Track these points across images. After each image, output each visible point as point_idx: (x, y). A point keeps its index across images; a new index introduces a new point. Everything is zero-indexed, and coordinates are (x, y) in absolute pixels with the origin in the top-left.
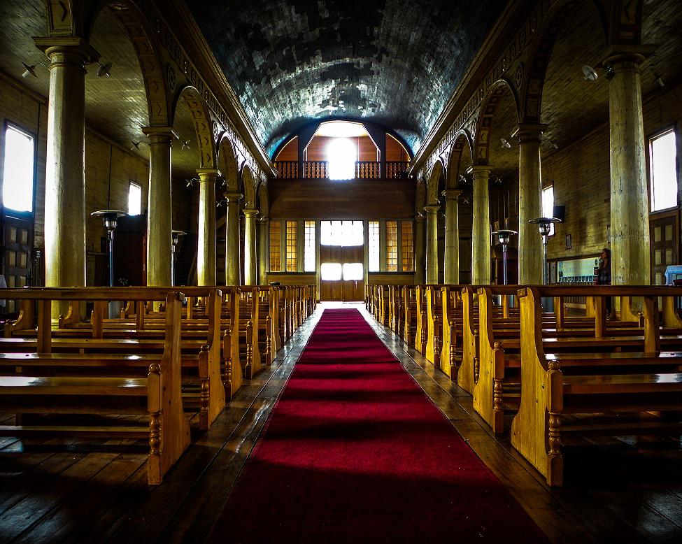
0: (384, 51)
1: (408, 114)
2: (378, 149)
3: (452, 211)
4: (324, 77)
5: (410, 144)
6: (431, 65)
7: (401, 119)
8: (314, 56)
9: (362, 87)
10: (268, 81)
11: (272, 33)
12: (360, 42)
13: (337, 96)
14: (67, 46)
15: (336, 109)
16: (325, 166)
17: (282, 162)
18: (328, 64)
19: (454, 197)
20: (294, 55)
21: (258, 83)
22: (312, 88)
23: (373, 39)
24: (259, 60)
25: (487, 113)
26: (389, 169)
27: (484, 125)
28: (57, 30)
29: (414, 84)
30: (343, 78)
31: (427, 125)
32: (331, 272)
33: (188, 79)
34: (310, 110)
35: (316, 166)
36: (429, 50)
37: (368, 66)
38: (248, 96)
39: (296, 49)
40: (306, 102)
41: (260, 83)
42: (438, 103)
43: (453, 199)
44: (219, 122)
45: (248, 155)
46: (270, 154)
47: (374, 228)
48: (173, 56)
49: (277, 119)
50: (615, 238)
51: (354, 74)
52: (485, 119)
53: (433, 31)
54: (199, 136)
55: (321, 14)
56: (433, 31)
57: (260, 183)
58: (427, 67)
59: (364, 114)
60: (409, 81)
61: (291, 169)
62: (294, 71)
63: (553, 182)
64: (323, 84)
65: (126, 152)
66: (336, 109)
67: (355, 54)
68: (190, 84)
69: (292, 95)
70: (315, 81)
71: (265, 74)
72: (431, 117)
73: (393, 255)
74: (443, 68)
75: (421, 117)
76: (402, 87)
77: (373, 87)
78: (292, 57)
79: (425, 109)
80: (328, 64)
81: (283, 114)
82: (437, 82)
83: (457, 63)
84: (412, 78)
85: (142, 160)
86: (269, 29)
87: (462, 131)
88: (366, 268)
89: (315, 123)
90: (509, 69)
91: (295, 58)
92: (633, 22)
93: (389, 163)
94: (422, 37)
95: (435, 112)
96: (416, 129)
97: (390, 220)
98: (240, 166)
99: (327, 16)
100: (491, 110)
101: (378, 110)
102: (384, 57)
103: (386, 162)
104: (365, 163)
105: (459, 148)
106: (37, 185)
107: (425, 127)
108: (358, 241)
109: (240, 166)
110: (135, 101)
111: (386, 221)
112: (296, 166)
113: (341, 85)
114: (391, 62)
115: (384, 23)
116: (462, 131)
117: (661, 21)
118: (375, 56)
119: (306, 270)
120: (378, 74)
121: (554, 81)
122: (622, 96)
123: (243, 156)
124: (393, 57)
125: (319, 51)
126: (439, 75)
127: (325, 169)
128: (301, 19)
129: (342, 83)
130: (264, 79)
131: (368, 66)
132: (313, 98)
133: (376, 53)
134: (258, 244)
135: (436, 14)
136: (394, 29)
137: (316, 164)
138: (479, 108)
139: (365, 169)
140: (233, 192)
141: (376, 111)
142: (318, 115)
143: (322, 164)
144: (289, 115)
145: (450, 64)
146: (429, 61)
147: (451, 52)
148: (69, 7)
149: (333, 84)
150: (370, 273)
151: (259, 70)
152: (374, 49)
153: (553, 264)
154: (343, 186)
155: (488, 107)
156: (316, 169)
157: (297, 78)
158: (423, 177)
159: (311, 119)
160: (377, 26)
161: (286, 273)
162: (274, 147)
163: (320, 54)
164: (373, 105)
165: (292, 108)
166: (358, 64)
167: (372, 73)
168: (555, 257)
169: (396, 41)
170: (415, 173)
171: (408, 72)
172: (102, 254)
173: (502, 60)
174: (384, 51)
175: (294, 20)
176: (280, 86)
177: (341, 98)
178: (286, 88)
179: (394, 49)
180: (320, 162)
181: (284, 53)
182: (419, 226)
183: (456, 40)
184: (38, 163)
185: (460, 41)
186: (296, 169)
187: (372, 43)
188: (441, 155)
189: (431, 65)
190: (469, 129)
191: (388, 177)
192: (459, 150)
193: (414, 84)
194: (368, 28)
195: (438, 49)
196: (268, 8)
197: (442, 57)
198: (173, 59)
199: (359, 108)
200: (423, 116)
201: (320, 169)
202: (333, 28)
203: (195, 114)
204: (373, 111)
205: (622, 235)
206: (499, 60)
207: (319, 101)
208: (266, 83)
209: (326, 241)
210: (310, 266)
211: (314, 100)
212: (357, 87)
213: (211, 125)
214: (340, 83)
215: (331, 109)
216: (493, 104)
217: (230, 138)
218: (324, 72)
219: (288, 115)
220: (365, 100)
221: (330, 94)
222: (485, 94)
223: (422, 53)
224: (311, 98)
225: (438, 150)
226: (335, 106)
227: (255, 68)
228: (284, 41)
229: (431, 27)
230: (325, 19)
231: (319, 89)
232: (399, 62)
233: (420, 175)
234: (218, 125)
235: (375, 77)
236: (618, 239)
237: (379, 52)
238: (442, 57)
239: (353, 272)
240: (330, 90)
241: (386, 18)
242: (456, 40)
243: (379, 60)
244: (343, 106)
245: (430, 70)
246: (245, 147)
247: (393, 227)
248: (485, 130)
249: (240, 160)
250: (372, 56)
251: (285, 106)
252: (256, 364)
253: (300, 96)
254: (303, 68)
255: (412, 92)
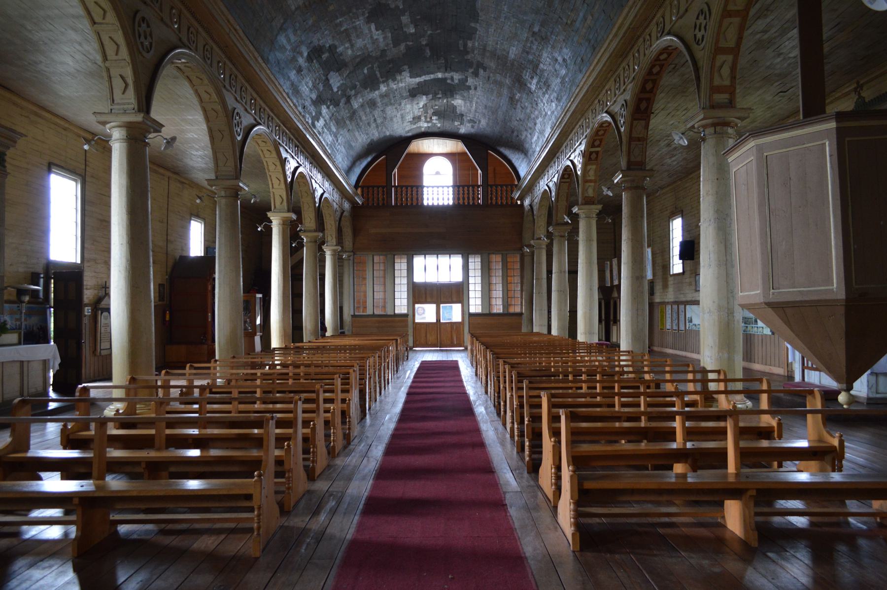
0: (480, 65)
1: (513, 132)
2: (480, 171)
3: (561, 250)
4: (414, 93)
5: (516, 163)
6: (535, 81)
7: (504, 137)
8: (400, 72)
9: (458, 102)
10: (348, 101)
11: (350, 52)
12: (453, 56)
13: (430, 111)
14: (130, 122)
15: (430, 125)
16: (417, 191)
17: (368, 187)
18: (418, 80)
19: (563, 234)
20: (377, 73)
21: (337, 104)
22: (400, 104)
23: (467, 53)
24: (336, 81)
25: (593, 146)
26: (491, 194)
27: (590, 159)
28: (118, 104)
29: (517, 101)
30: (435, 94)
31: (534, 146)
32: (426, 313)
33: (255, 119)
34: (400, 127)
35: (407, 192)
36: (531, 67)
37: (463, 82)
38: (325, 121)
39: (379, 67)
40: (394, 119)
41: (338, 105)
42: (544, 123)
43: (561, 236)
44: (293, 157)
45: (327, 184)
46: (354, 178)
47: (475, 263)
48: (238, 99)
49: (360, 140)
50: (704, 314)
51: (449, 90)
52: (591, 153)
53: (535, 47)
54: (270, 176)
55: (405, 29)
56: (535, 47)
57: (342, 213)
58: (531, 84)
59: (463, 130)
60: (512, 99)
61: (378, 194)
62: (378, 89)
63: (682, 211)
64: (412, 101)
65: (186, 183)
66: (430, 125)
67: (447, 68)
68: (259, 124)
69: (377, 113)
70: (402, 98)
71: (344, 94)
72: (538, 137)
73: (498, 293)
74: (548, 86)
75: (526, 136)
76: (504, 101)
77: (471, 102)
78: (376, 75)
79: (531, 128)
80: (418, 80)
81: (367, 134)
82: (542, 101)
83: (563, 82)
84: (514, 95)
85: (204, 190)
86: (347, 48)
87: (569, 163)
88: (466, 309)
89: (407, 140)
90: (613, 104)
91: (379, 75)
92: (727, 83)
93: (491, 186)
94: (522, 53)
95: (542, 132)
96: (521, 148)
97: (493, 253)
98: (317, 200)
99: (413, 31)
100: (597, 143)
101: (478, 127)
102: (481, 71)
103: (488, 185)
104: (463, 187)
105: (568, 178)
106: (86, 233)
107: (532, 148)
108: (457, 276)
109: (317, 200)
110: (195, 136)
111: (489, 254)
112: (383, 191)
113: (433, 101)
114: (489, 77)
115: (479, 38)
116: (569, 163)
117: (782, 54)
118: (471, 70)
119: (396, 312)
120: (476, 89)
121: (668, 112)
122: (714, 164)
123: (320, 186)
124: (491, 72)
125: (406, 67)
126: (544, 94)
127: (417, 194)
128: (383, 36)
129: (435, 98)
130: (343, 101)
131: (463, 82)
132: (402, 115)
133: (471, 68)
134: (341, 294)
135: (536, 29)
136: (490, 43)
137: (407, 188)
138: (585, 140)
139: (463, 194)
140: (310, 231)
141: (476, 127)
142: (408, 132)
143: (414, 189)
144: (375, 134)
145: (555, 83)
146: (532, 78)
147: (556, 70)
148: (130, 81)
149: (423, 101)
150: (471, 315)
151: (338, 91)
152: (469, 64)
153: (682, 307)
154: (438, 212)
155: (594, 141)
156: (407, 195)
157: (382, 96)
158: (531, 205)
159: (401, 137)
160: (471, 40)
161: (374, 315)
162: (358, 170)
163: (408, 70)
164: (471, 121)
165: (377, 127)
166: (452, 79)
167: (469, 88)
168: (684, 299)
169: (493, 54)
170: (522, 198)
171: (509, 88)
172: (161, 302)
173: (607, 92)
174: (480, 65)
175: (375, 37)
176: (362, 106)
177: (435, 114)
178: (370, 107)
179: (493, 65)
180: (412, 187)
181: (366, 71)
182: (527, 260)
183: (560, 59)
184: (87, 207)
185: (564, 60)
186: (383, 195)
187: (466, 57)
188: (550, 181)
189: (535, 81)
190: (576, 161)
191: (491, 203)
192: (567, 180)
193: (517, 101)
194: (461, 42)
195: (541, 66)
196: (344, 28)
197: (546, 75)
198: (239, 102)
199: (456, 123)
200: (529, 136)
201: (412, 194)
202: (421, 42)
203: (264, 152)
204: (473, 127)
205: (710, 312)
206: (604, 91)
207: (409, 118)
208: (346, 104)
209: (419, 278)
210: (401, 305)
211: (402, 117)
212: (453, 102)
213: (283, 162)
214: (432, 99)
215: (424, 125)
216: (599, 138)
217: (305, 173)
218: (413, 88)
219: (373, 134)
220: (462, 115)
221: (422, 110)
222: (591, 127)
223: (524, 69)
224: (399, 115)
225: (546, 177)
226: (428, 122)
227: (332, 90)
228: (364, 59)
229: (532, 42)
230: (412, 34)
231: (408, 106)
232: (498, 77)
233: (527, 202)
234: (291, 160)
235: (472, 92)
236: (707, 316)
237: (475, 66)
238: (546, 75)
239: (454, 313)
240: (421, 106)
241: (481, 31)
242: (560, 59)
243: (476, 74)
244: (437, 122)
245: (533, 87)
246: (323, 177)
247: (497, 261)
248: (592, 164)
249: (319, 192)
250: (468, 71)
251: (369, 124)
252: (338, 442)
253: (386, 114)
254: (388, 85)
255: (515, 109)
